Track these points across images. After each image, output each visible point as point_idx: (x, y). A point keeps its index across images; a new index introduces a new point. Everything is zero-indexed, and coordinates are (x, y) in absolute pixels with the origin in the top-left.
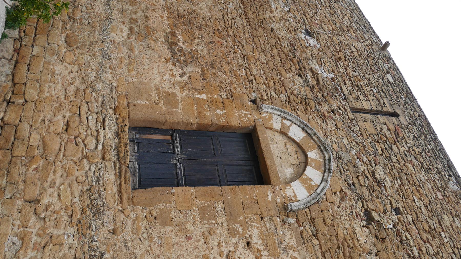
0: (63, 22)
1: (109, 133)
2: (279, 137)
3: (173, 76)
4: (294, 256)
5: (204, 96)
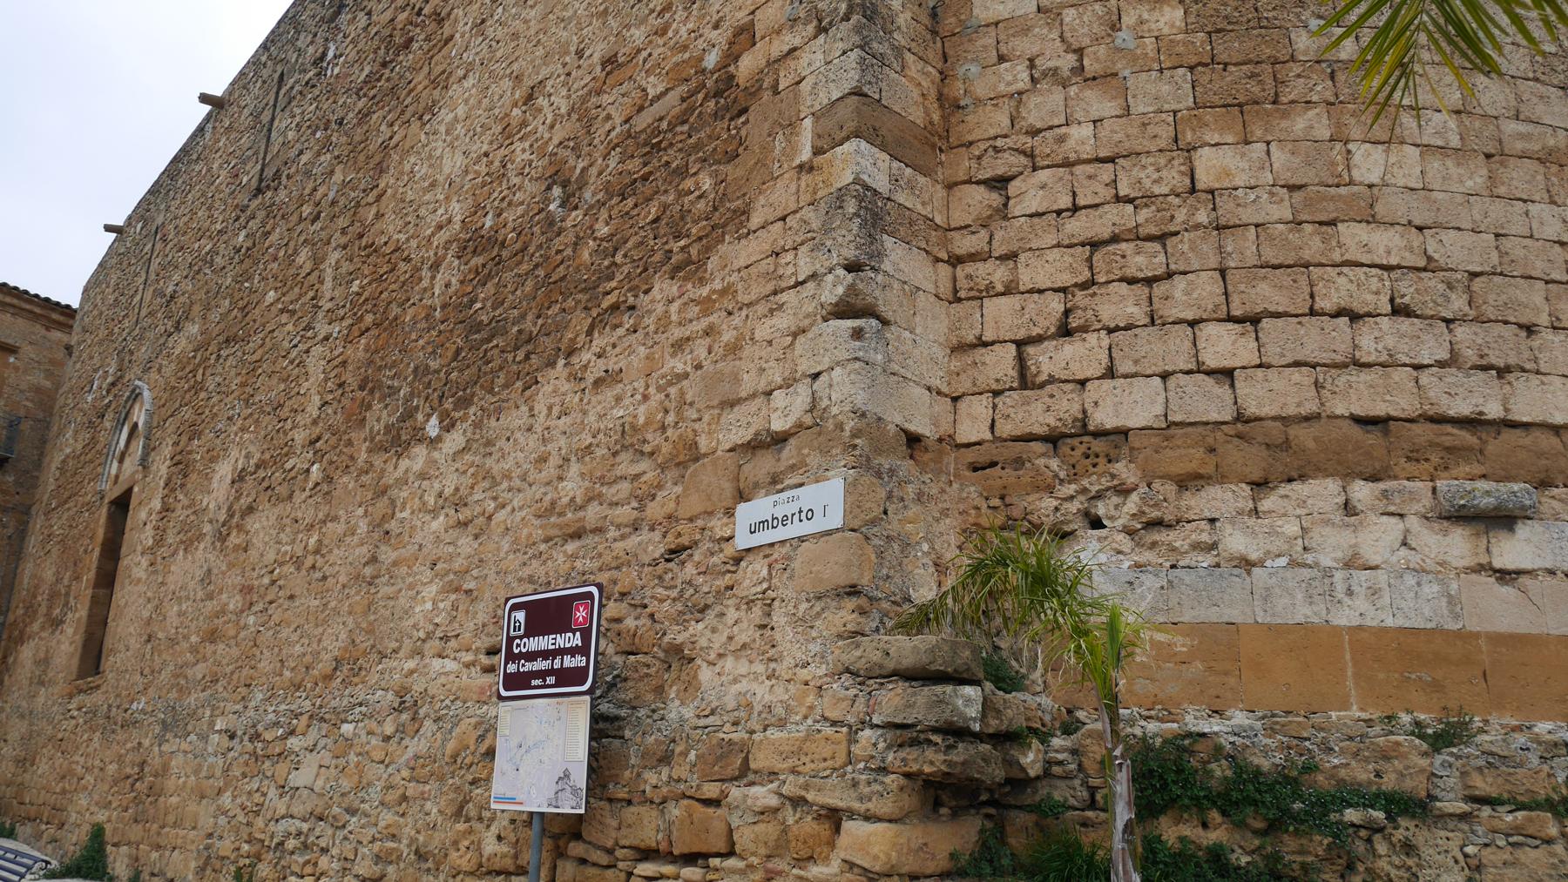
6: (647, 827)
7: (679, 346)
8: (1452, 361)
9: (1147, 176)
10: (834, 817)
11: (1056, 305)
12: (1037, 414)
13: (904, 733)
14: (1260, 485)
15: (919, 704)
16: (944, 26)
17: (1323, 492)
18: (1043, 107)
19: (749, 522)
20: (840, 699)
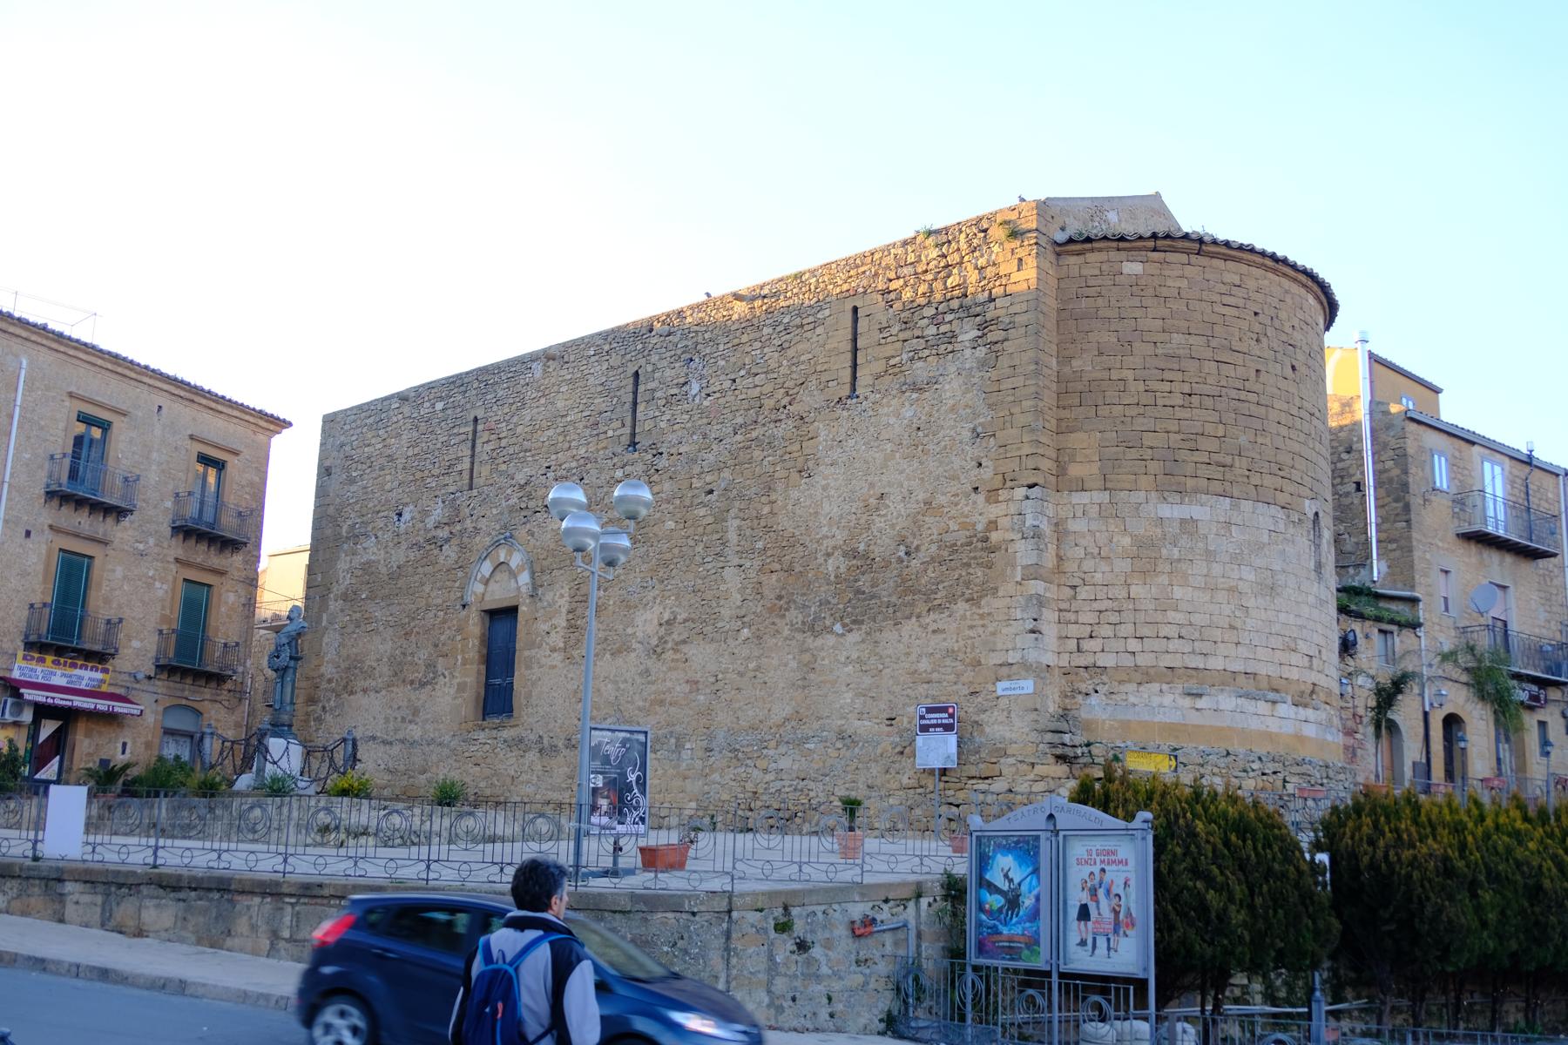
0: (866, 983)
1: (482, 736)
2: (492, 586)
6: (973, 771)
7: (971, 627)
8: (1193, 652)
10: (1033, 765)
11: (1089, 629)
13: (1052, 745)
15: (1056, 738)
16: (1205, 1037)
17: (1155, 687)
18: (1088, 565)
19: (1001, 687)
20: (1034, 736)
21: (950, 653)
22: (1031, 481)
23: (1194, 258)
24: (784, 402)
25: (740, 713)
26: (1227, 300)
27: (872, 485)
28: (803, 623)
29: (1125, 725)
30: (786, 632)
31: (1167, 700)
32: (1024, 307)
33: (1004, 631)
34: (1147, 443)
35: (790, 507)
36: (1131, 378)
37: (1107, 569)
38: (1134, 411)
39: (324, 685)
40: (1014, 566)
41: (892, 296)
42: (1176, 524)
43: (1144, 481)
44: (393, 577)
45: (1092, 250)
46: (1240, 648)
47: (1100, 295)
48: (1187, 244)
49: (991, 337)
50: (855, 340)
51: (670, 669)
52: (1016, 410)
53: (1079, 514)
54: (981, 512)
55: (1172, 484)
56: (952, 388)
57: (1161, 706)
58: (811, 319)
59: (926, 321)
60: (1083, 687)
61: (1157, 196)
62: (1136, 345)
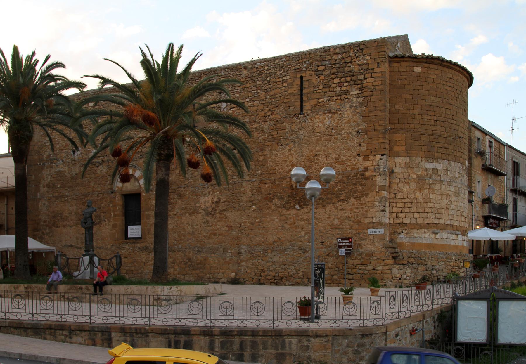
1: (127, 246)
3: (106, 224)
4: (361, 293)
5: (112, 213)
7: (357, 208)
8: (435, 218)
9: (411, 196)
10: (384, 260)
11: (401, 209)
12: (398, 221)
13: (392, 253)
14: (418, 229)
15: (393, 250)
17: (423, 230)
18: (401, 185)
19: (370, 231)
21: (349, 218)
22: (383, 153)
23: (439, 67)
24: (268, 114)
25: (252, 239)
26: (449, 84)
27: (311, 151)
28: (281, 204)
29: (413, 244)
30: (273, 207)
31: (427, 235)
32: (380, 83)
33: (371, 210)
34: (422, 139)
35: (273, 158)
36: (417, 113)
37: (407, 187)
38: (418, 127)
39: (42, 223)
40: (375, 186)
41: (319, 72)
42: (431, 170)
43: (421, 153)
44: (73, 178)
45: (403, 61)
46: (449, 216)
47: (406, 79)
48: (437, 61)
49: (365, 94)
50: (301, 91)
51: (218, 221)
52: (376, 124)
53: (397, 166)
54: (361, 164)
55: (430, 157)
56: (347, 113)
57: (425, 237)
58: (281, 79)
59: (335, 85)
60: (398, 231)
61: (407, 35)
62: (419, 100)
